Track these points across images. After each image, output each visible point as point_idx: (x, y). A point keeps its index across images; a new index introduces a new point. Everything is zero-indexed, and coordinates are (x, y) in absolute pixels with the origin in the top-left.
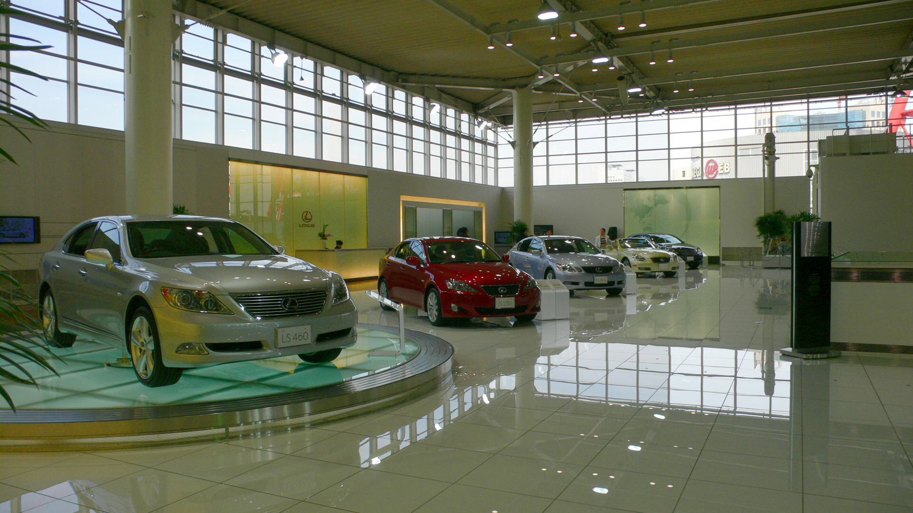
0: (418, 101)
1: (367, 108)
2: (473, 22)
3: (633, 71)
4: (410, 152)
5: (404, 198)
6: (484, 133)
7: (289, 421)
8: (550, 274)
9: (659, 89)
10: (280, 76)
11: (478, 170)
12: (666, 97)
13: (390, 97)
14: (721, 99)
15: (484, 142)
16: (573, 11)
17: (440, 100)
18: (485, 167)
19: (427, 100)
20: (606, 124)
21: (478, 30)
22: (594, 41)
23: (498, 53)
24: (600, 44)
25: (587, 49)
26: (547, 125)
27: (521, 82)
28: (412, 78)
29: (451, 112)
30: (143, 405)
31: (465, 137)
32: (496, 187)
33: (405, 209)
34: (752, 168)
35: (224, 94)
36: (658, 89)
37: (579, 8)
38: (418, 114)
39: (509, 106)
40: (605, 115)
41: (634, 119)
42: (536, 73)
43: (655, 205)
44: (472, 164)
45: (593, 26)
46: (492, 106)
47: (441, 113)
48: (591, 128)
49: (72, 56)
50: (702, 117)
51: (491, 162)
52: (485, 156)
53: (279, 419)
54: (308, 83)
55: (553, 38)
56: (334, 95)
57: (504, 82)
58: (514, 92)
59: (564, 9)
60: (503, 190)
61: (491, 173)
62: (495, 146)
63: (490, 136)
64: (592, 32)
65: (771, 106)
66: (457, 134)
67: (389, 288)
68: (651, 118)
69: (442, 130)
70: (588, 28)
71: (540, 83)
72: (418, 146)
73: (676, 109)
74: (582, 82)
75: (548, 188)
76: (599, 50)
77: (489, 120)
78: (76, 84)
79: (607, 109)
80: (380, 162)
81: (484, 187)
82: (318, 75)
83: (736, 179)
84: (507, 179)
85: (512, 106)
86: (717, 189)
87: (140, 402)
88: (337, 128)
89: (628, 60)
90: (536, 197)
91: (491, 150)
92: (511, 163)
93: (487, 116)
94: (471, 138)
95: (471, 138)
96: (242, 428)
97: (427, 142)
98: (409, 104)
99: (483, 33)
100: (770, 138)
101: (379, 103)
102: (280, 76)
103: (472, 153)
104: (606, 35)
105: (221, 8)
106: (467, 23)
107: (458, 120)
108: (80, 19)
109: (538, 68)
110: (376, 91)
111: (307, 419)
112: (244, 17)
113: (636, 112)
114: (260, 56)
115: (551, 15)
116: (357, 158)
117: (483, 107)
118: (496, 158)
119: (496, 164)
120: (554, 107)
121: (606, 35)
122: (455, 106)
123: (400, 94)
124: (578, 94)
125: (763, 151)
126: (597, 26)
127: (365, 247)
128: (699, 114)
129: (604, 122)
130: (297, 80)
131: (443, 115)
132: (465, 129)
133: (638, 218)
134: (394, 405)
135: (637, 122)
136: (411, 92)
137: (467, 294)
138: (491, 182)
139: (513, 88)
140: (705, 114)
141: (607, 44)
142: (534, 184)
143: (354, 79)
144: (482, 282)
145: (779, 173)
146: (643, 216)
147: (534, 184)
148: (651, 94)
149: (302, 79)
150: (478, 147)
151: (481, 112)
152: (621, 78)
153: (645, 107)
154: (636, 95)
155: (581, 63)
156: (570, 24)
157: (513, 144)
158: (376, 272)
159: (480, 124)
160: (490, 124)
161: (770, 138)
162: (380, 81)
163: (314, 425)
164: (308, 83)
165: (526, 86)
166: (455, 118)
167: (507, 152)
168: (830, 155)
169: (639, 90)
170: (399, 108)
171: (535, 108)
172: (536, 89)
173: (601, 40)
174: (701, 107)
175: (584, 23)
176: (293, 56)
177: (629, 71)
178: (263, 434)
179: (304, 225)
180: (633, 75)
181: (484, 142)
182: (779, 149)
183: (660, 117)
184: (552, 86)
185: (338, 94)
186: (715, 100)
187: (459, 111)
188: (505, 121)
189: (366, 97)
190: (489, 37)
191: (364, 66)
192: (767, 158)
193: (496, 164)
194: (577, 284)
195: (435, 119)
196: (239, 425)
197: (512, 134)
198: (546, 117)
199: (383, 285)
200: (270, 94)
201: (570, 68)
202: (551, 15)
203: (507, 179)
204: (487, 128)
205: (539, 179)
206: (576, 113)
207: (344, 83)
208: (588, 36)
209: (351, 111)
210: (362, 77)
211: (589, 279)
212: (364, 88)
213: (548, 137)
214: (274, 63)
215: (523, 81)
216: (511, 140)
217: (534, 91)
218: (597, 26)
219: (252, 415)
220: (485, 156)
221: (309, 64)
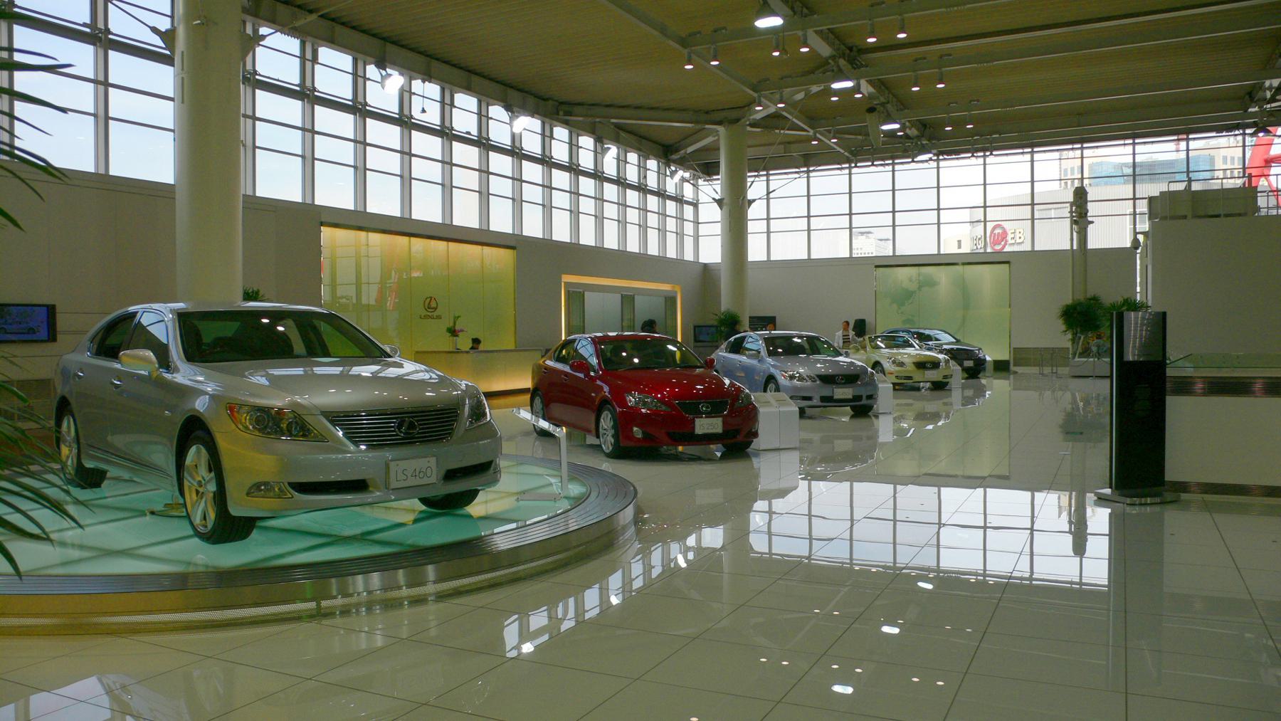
0: (586, 142)
1: (516, 152)
2: (663, 31)
3: (889, 100)
4: (575, 213)
5: (567, 278)
6: (680, 186)
7: (405, 592)
8: (772, 386)
9: (925, 126)
10: (393, 107)
11: (671, 239)
12: (935, 136)
13: (547, 137)
14: (1012, 139)
15: (679, 200)
16: (803, 16)
17: (617, 140)
18: (680, 235)
19: (599, 140)
20: (850, 174)
21: (671, 43)
22: (833, 57)
23: (699, 74)
24: (842, 62)
25: (824, 69)
26: (768, 175)
27: (732, 115)
28: (577, 109)
29: (633, 157)
30: (201, 569)
31: (652, 193)
32: (696, 263)
33: (568, 294)
34: (1056, 236)
35: (314, 132)
36: (923, 125)
37: (812, 12)
38: (586, 160)
39: (714, 149)
40: (849, 161)
41: (890, 168)
42: (752, 103)
43: (920, 288)
44: (662, 231)
45: (832, 36)
46: (690, 150)
47: (618, 159)
48: (829, 180)
49: (101, 78)
50: (985, 164)
51: (689, 228)
52: (680, 219)
53: (392, 589)
54: (433, 117)
55: (776, 54)
56: (468, 133)
57: (707, 115)
58: (721, 129)
59: (791, 13)
60: (706, 266)
61: (688, 243)
62: (695, 205)
63: (688, 191)
64: (831, 44)
65: (1082, 148)
66: (642, 189)
67: (546, 405)
68: (913, 165)
69: (621, 182)
70: (826, 39)
71: (758, 116)
72: (587, 205)
73: (949, 153)
74: (817, 115)
75: (769, 264)
76: (840, 70)
77: (686, 168)
78: (107, 118)
79: (851, 153)
80: (533, 227)
81: (679, 262)
82: (447, 105)
83: (1033, 252)
84: (712, 251)
85: (718, 149)
86: (1007, 266)
87: (196, 565)
88: (472, 180)
89: (880, 85)
90: (751, 277)
91: (689, 211)
92: (717, 229)
93: (683, 163)
94: (661, 194)
95: (661, 194)
96: (339, 601)
97: (600, 199)
98: (573, 147)
99: (677, 46)
100: (1081, 194)
101: (532, 144)
102: (393, 107)
103: (663, 215)
104: (851, 49)
105: (311, 12)
106: (655, 33)
107: (642, 169)
108: (112, 27)
109: (755, 95)
110: (528, 128)
111: (430, 588)
112: (343, 24)
113: (893, 158)
114: (365, 79)
115: (774, 22)
116: (501, 222)
117: (677, 151)
118: (697, 223)
119: (696, 230)
120: (777, 150)
121: (851, 49)
122: (638, 149)
123: (561, 133)
124: (811, 133)
125: (1071, 212)
126: (837, 37)
127: (512, 347)
128: (981, 161)
129: (847, 171)
130: (416, 113)
131: (622, 162)
132: (652, 182)
133: (895, 306)
134: (553, 570)
135: (893, 171)
136: (576, 129)
137: (655, 413)
138: (689, 256)
139: (720, 123)
140: (989, 160)
141: (852, 61)
142: (750, 259)
143: (497, 111)
144: (676, 396)
145: (1093, 244)
146: (903, 304)
147: (750, 259)
148: (913, 132)
149: (424, 111)
150: (671, 207)
151: (674, 157)
152: (871, 110)
153: (905, 151)
154: (892, 133)
155: (815, 89)
156: (800, 33)
157: (720, 202)
158: (527, 383)
159: (673, 174)
160: (687, 175)
161: (1081, 194)
162: (533, 114)
163: (441, 597)
164: (433, 117)
165: (738, 120)
166: (639, 166)
167: (712, 214)
168: (1164, 218)
169: (897, 126)
170: (560, 152)
171: (751, 152)
172: (752, 125)
173: (843, 56)
174: (984, 150)
175: (819, 33)
176: (411, 79)
177: (882, 99)
178: (369, 609)
179: (426, 317)
180: (889, 106)
181: (679, 200)
182: (1092, 209)
183: (926, 165)
184: (774, 121)
185: (475, 132)
186: (1004, 140)
187: (644, 155)
188: (709, 170)
189: (513, 136)
190: (686, 51)
191: (511, 92)
192: (1075, 222)
193: (696, 230)
194: (809, 399)
195: (610, 167)
196: (335, 597)
197: (718, 188)
198: (766, 164)
199: (538, 401)
200: (379, 132)
201: (800, 96)
202: (774, 22)
203: (712, 251)
204: (683, 180)
205: (756, 252)
206: (809, 159)
207: (483, 117)
208: (825, 50)
209: (493, 156)
210: (508, 108)
211: (826, 393)
212: (511, 124)
213: (768, 193)
214: (385, 89)
215: (734, 114)
216: (717, 197)
217: (749, 128)
218: (837, 37)
219: (354, 583)
220: (680, 219)
221: (433, 90)
